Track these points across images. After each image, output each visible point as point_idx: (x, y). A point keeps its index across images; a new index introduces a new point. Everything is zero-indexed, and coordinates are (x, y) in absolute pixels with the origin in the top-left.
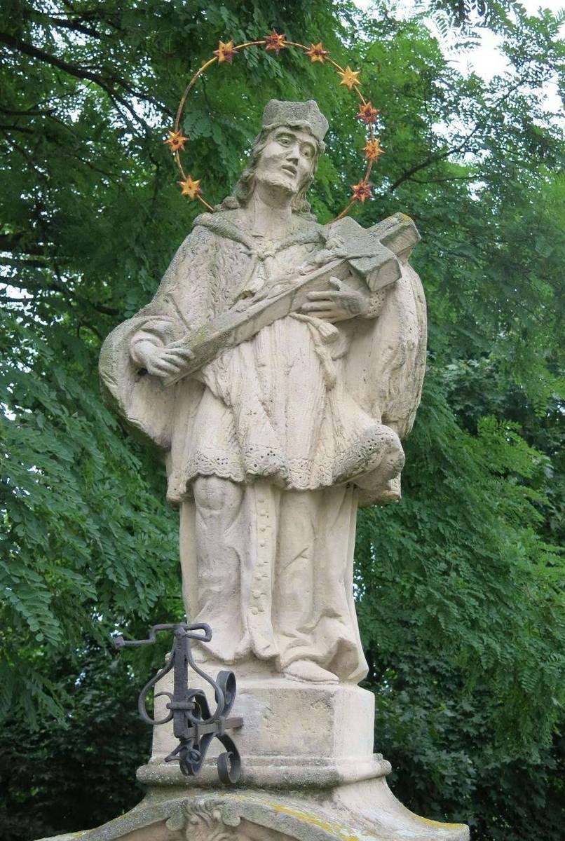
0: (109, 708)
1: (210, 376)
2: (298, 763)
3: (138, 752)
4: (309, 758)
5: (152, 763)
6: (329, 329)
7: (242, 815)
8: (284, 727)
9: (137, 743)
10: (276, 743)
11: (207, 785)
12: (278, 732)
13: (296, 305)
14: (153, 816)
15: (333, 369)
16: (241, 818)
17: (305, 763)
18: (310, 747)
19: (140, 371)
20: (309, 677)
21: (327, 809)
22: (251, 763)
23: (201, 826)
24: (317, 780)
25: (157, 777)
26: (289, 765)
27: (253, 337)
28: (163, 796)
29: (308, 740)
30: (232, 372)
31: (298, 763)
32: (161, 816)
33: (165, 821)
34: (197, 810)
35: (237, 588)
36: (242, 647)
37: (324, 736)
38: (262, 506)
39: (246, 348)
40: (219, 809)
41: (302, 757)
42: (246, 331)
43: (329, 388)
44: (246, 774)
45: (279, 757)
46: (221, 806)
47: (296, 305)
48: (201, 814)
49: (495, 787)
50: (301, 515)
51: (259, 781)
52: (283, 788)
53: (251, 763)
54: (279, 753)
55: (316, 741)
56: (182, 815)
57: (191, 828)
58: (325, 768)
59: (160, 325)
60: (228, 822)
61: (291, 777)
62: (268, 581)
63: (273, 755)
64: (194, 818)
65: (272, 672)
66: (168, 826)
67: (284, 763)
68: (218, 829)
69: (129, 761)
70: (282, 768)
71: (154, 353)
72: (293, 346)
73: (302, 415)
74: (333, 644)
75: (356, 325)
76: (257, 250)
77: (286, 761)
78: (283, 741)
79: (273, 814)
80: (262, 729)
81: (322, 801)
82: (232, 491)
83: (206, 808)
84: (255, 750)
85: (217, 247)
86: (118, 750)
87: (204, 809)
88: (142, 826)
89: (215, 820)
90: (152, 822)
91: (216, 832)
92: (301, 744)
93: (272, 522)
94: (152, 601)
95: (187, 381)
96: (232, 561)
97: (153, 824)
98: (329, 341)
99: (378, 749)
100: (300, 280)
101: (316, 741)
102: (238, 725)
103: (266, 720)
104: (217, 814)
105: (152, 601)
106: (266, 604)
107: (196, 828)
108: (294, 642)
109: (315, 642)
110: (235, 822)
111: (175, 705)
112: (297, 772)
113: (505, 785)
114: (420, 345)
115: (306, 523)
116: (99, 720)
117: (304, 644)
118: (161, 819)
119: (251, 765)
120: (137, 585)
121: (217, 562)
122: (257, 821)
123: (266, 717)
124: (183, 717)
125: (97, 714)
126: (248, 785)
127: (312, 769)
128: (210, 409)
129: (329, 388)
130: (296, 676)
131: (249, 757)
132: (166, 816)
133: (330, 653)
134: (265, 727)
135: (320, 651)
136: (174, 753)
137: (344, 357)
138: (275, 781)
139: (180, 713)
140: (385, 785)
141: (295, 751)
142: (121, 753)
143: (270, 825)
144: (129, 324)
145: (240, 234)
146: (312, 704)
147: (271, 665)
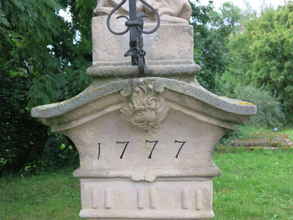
2: (176, 63)
3: (10, 92)
4: (181, 60)
5: (94, 66)
7: (165, 86)
8: (167, 45)
9: (9, 89)
10: (162, 54)
11: (126, 76)
12: (163, 48)
14: (112, 89)
16: (165, 88)
17: (179, 63)
18: (181, 55)
20: (174, 21)
22: (150, 64)
23: (141, 93)
24: (187, 71)
25: (98, 72)
26: (171, 64)
28: (101, 83)
29: (180, 52)
31: (176, 63)
32: (118, 89)
33: (120, 91)
34: (139, 84)
37: (188, 50)
40: (152, 84)
41: (177, 60)
44: (149, 69)
45: (163, 61)
46: (153, 82)
48: (142, 86)
51: (156, 73)
53: (150, 64)
54: (164, 59)
55: (184, 52)
56: (130, 88)
57: (135, 94)
58: (191, 65)
60: (157, 90)
61: (173, 70)
63: (160, 60)
64: (138, 89)
65: (151, 20)
66: (122, 94)
67: (167, 63)
68: (150, 94)
69: (7, 95)
70: (167, 66)
74: (181, 6)
77: (169, 62)
78: (166, 53)
79: (182, 85)
80: (154, 46)
81: (189, 82)
83: (145, 83)
84: (150, 58)
86: (2, 91)
87: (143, 84)
88: (105, 95)
89: (150, 89)
90: (111, 93)
91: (149, 96)
92: (175, 54)
94: (35, 18)
97: (113, 93)
101: (184, 52)
103: (155, 42)
104: (151, 86)
105: (35, 18)
107: (138, 94)
108: (162, 4)
109: (170, 6)
110: (161, 90)
111: (131, 22)
117: (166, 7)
118: (117, 90)
119: (150, 65)
120: (28, 10)
122: (173, 89)
123: (156, 41)
124: (136, 30)
126: (151, 74)
127: (185, 66)
130: (166, 21)
131: (148, 61)
132: (121, 89)
133: (179, 11)
134: (156, 46)
136: (129, 52)
138: (165, 72)
139: (134, 27)
141: (173, 57)
142: (4, 92)
143: (180, 91)
146: (181, 33)
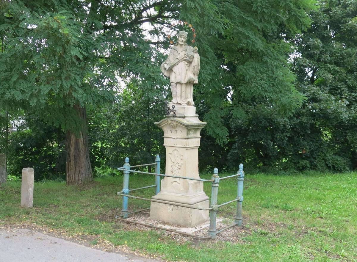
0: (204, 108)
1: (173, 69)
6: (186, 63)
13: (182, 60)
15: (187, 68)
19: (165, 68)
21: (184, 119)
27: (178, 64)
30: (175, 69)
35: (176, 96)
36: (176, 102)
38: (178, 86)
39: (177, 66)
42: (177, 64)
43: (187, 71)
47: (182, 60)
49: (296, 127)
50: (184, 87)
52: (180, 117)
59: (167, 63)
62: (180, 95)
71: (167, 67)
72: (182, 65)
73: (183, 75)
75: (190, 63)
76: (179, 52)
82: (175, 84)
85: (174, 51)
93: (180, 88)
95: (171, 70)
96: (175, 92)
98: (187, 65)
99: (196, 113)
100: (183, 57)
102: (176, 111)
106: (180, 97)
112: (181, 115)
113: (297, 127)
114: (198, 64)
115: (185, 88)
116: (202, 111)
119: (177, 115)
121: (194, 82)
125: (201, 110)
126: (175, 117)
128: (173, 74)
129: (187, 71)
135: (186, 102)
137: (189, 66)
140: (198, 118)
144: (163, 63)
145: (177, 50)
147: (180, 104)
